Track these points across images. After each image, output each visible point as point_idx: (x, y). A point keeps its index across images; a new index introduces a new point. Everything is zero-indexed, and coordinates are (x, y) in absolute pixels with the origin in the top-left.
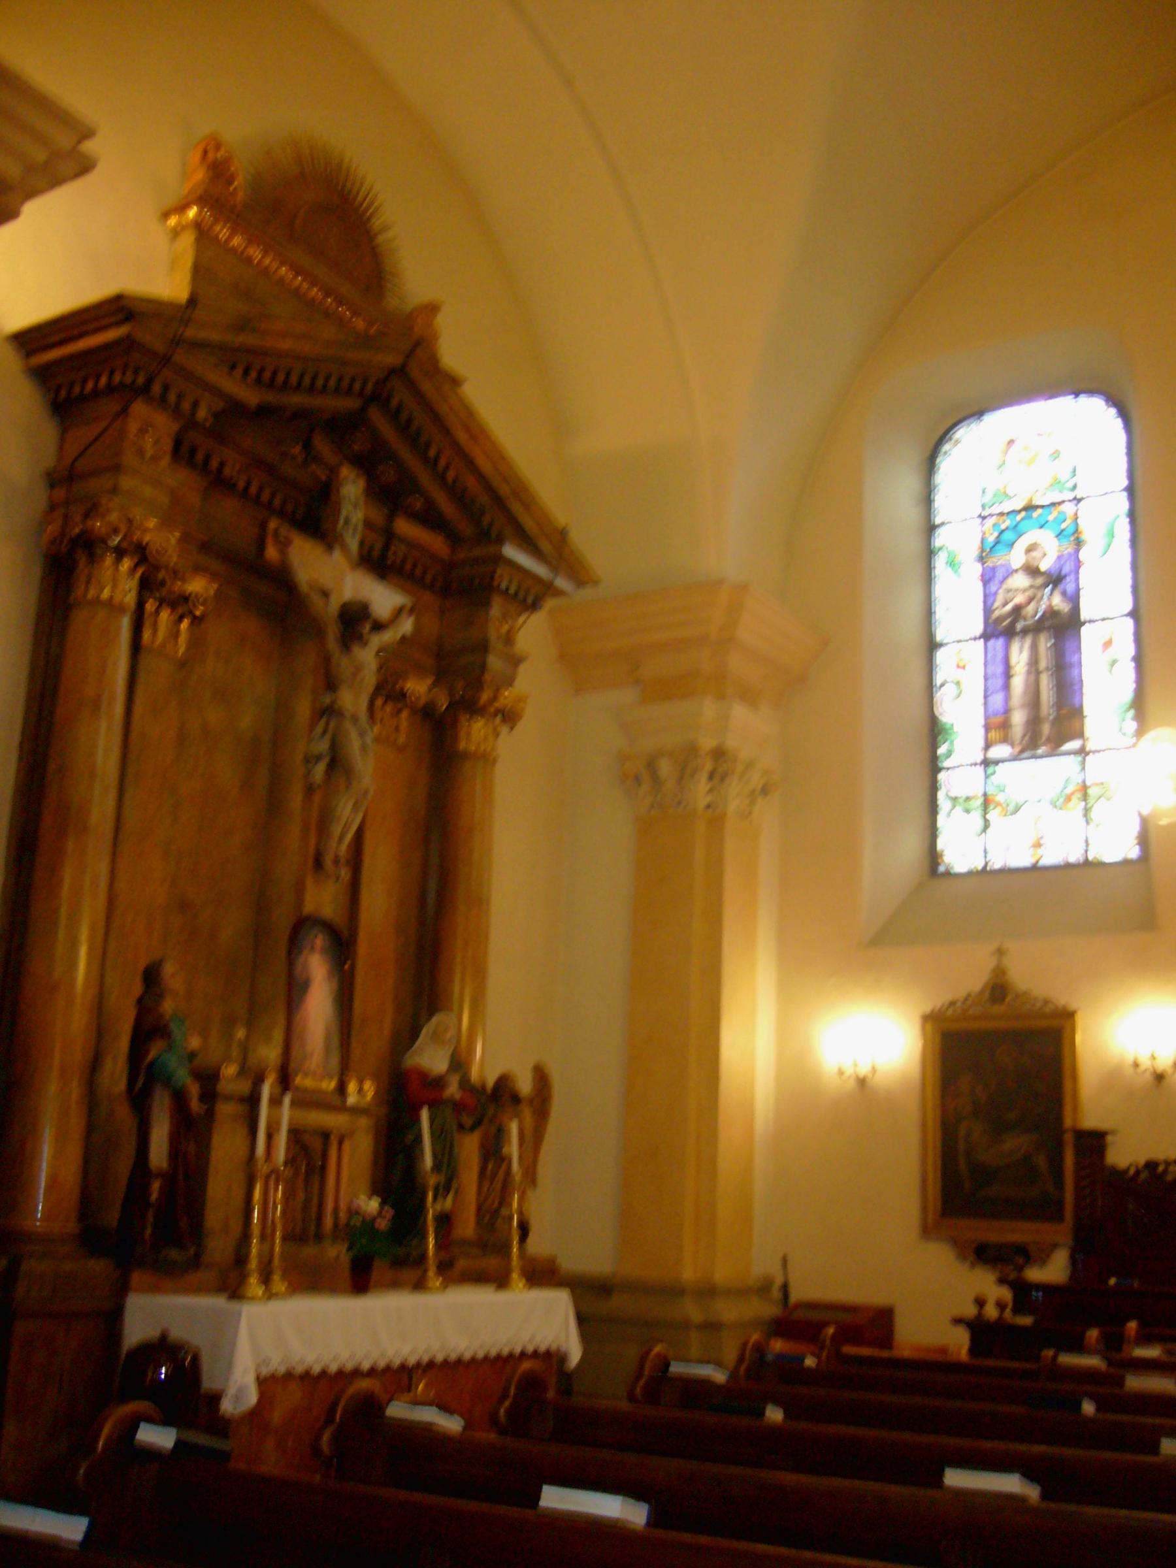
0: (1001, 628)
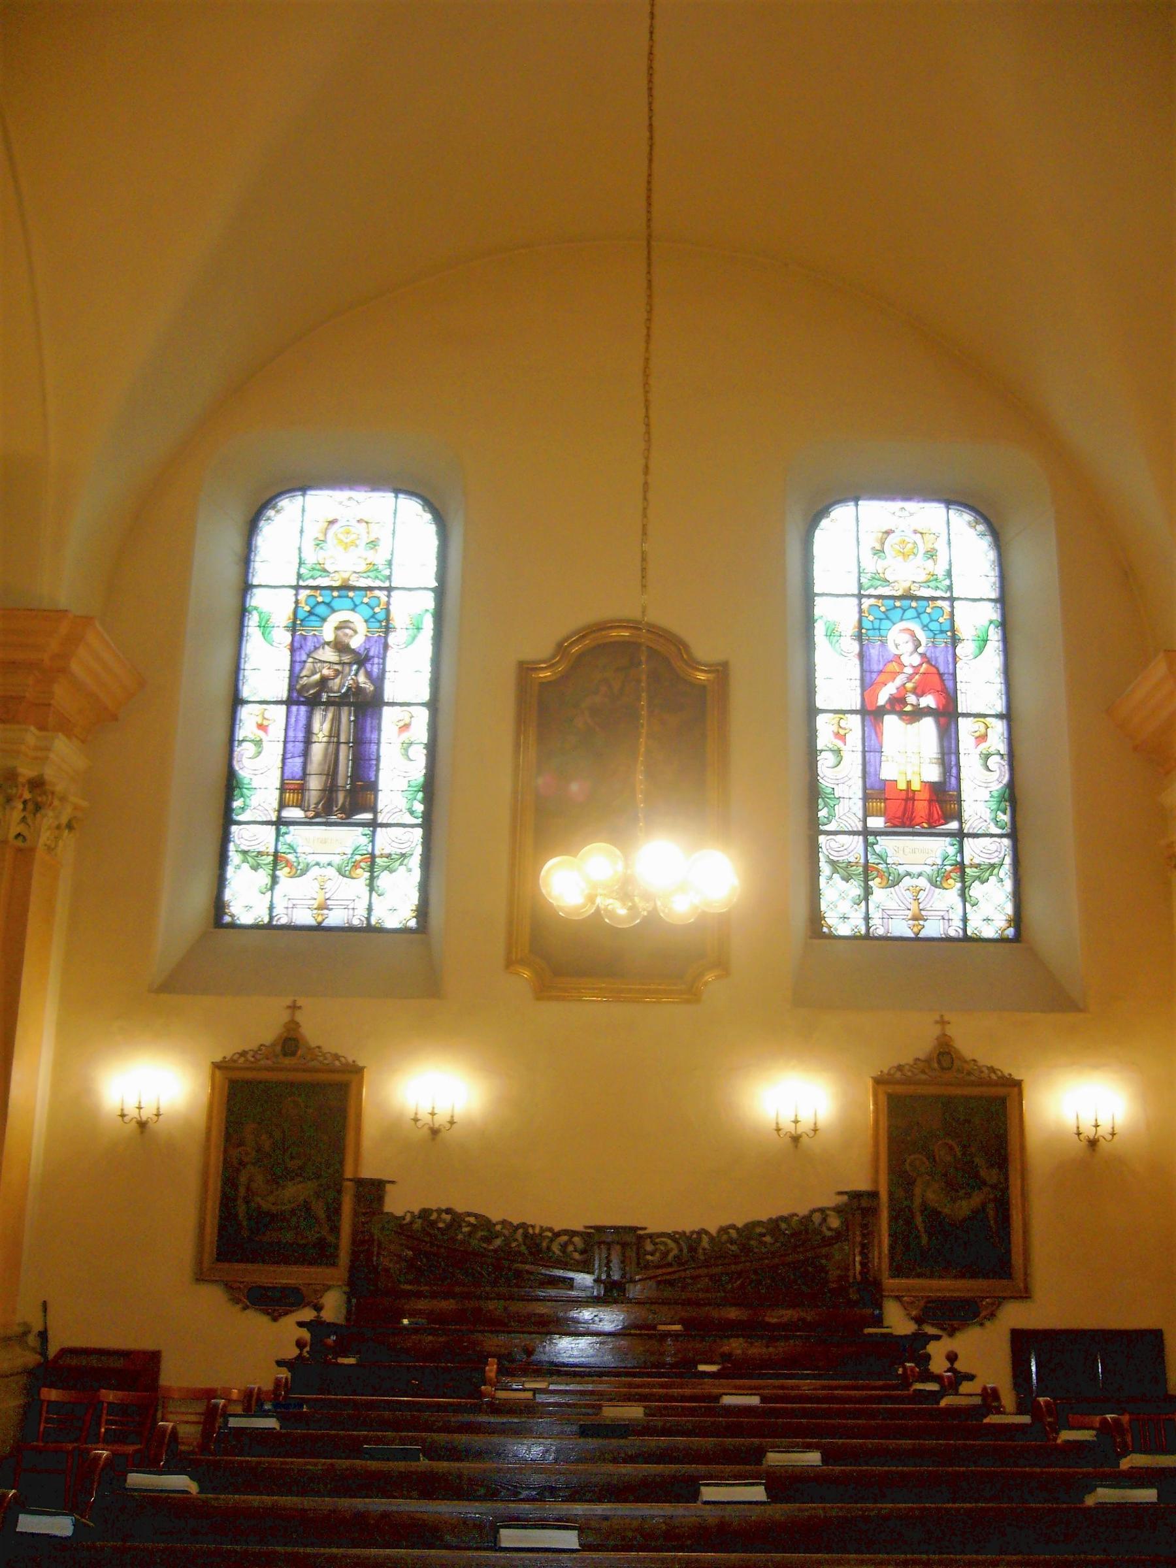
0: (304, 696)
